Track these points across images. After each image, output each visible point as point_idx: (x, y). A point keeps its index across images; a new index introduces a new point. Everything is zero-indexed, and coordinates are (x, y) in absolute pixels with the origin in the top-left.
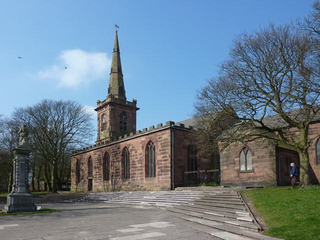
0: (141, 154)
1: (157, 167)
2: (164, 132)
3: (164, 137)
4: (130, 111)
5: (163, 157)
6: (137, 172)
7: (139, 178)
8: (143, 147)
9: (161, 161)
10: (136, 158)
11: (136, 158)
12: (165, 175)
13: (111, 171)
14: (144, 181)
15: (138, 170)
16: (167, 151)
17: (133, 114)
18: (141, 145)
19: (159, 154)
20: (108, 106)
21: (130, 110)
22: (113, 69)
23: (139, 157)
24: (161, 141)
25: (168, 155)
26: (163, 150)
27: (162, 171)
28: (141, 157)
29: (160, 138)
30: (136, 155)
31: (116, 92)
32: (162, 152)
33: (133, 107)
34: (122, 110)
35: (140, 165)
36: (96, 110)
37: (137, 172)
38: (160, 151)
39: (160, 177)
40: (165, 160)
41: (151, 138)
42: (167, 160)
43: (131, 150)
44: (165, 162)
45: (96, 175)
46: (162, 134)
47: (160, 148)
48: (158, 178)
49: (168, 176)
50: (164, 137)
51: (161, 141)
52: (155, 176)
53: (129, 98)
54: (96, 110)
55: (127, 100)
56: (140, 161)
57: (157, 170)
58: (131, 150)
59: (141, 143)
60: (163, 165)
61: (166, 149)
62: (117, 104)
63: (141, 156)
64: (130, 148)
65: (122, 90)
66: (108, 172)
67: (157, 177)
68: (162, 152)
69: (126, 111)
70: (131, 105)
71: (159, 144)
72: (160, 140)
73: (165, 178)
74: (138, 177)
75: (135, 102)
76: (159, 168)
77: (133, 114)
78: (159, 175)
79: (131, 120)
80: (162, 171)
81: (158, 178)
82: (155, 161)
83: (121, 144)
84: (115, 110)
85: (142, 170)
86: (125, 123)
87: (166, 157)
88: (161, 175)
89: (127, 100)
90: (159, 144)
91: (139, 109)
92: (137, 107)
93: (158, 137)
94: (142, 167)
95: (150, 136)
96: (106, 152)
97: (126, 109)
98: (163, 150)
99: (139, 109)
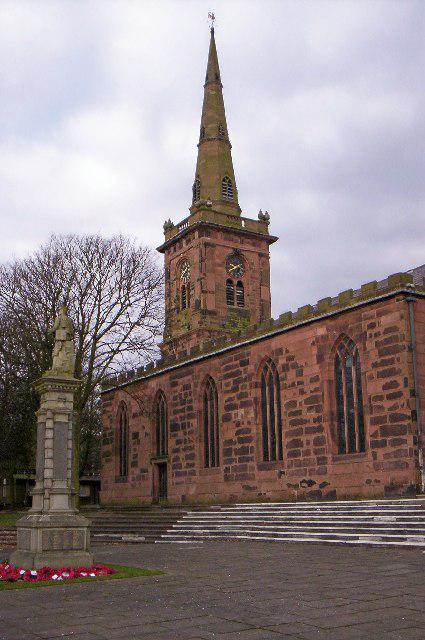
0: (315, 379)
1: (368, 418)
2: (384, 307)
3: (386, 321)
4: (252, 248)
5: (385, 388)
6: (304, 438)
7: (313, 457)
8: (320, 359)
9: (380, 398)
10: (302, 392)
11: (302, 392)
12: (395, 443)
13: (228, 433)
14: (329, 466)
15: (310, 431)
16: (396, 366)
17: (260, 255)
18: (315, 351)
19: (371, 377)
20: (197, 233)
21: (254, 245)
22: (206, 131)
23: (309, 388)
24: (376, 335)
25: (400, 380)
26: (384, 363)
27: (385, 431)
28: (316, 390)
29: (372, 326)
30: (300, 383)
31: (212, 197)
32: (381, 369)
33: (259, 235)
34: (231, 245)
35: (314, 414)
36: (161, 250)
37: (304, 438)
38: (375, 365)
39: (380, 452)
40: (390, 397)
41: (345, 327)
42: (399, 395)
43: (285, 368)
44: (391, 403)
45: (176, 451)
46: (380, 315)
47: (374, 357)
48: (374, 455)
49: (404, 447)
50: (386, 321)
51: (376, 335)
52: (362, 449)
53: (249, 210)
54: (161, 250)
55: (242, 215)
56: (314, 402)
57: (370, 429)
58: (285, 368)
59: (313, 344)
60: (386, 413)
61: (392, 361)
62: (218, 229)
63: (317, 385)
64: (282, 361)
65: (228, 184)
66: (215, 440)
67: (370, 451)
68: (381, 369)
69: (239, 247)
70: (255, 229)
71: (370, 345)
72: (375, 331)
73: (396, 454)
74: (307, 453)
75: (264, 219)
76: (375, 422)
77: (260, 255)
78: (375, 445)
79: (257, 275)
80: (385, 431)
81: (374, 455)
82: (360, 400)
83: (253, 348)
84: (213, 246)
85: (320, 429)
86: (240, 284)
87: (394, 384)
88: (383, 444)
89: (242, 215)
90: (370, 345)
91: (273, 240)
92: (249, 210)
93: (365, 324)
94: (318, 420)
95: (341, 320)
96: (160, 391)
97: (242, 242)
98: (384, 363)
99: (273, 240)
